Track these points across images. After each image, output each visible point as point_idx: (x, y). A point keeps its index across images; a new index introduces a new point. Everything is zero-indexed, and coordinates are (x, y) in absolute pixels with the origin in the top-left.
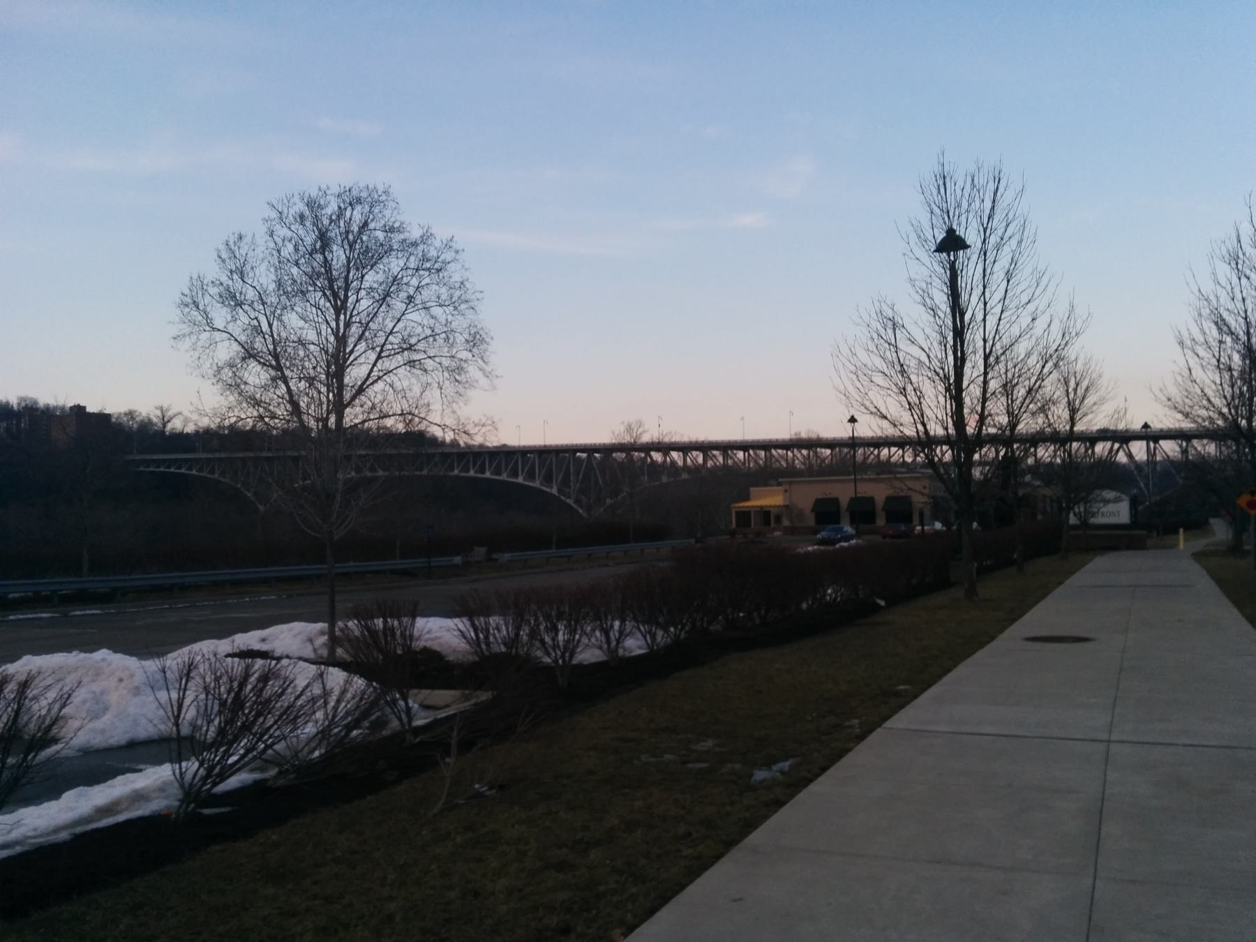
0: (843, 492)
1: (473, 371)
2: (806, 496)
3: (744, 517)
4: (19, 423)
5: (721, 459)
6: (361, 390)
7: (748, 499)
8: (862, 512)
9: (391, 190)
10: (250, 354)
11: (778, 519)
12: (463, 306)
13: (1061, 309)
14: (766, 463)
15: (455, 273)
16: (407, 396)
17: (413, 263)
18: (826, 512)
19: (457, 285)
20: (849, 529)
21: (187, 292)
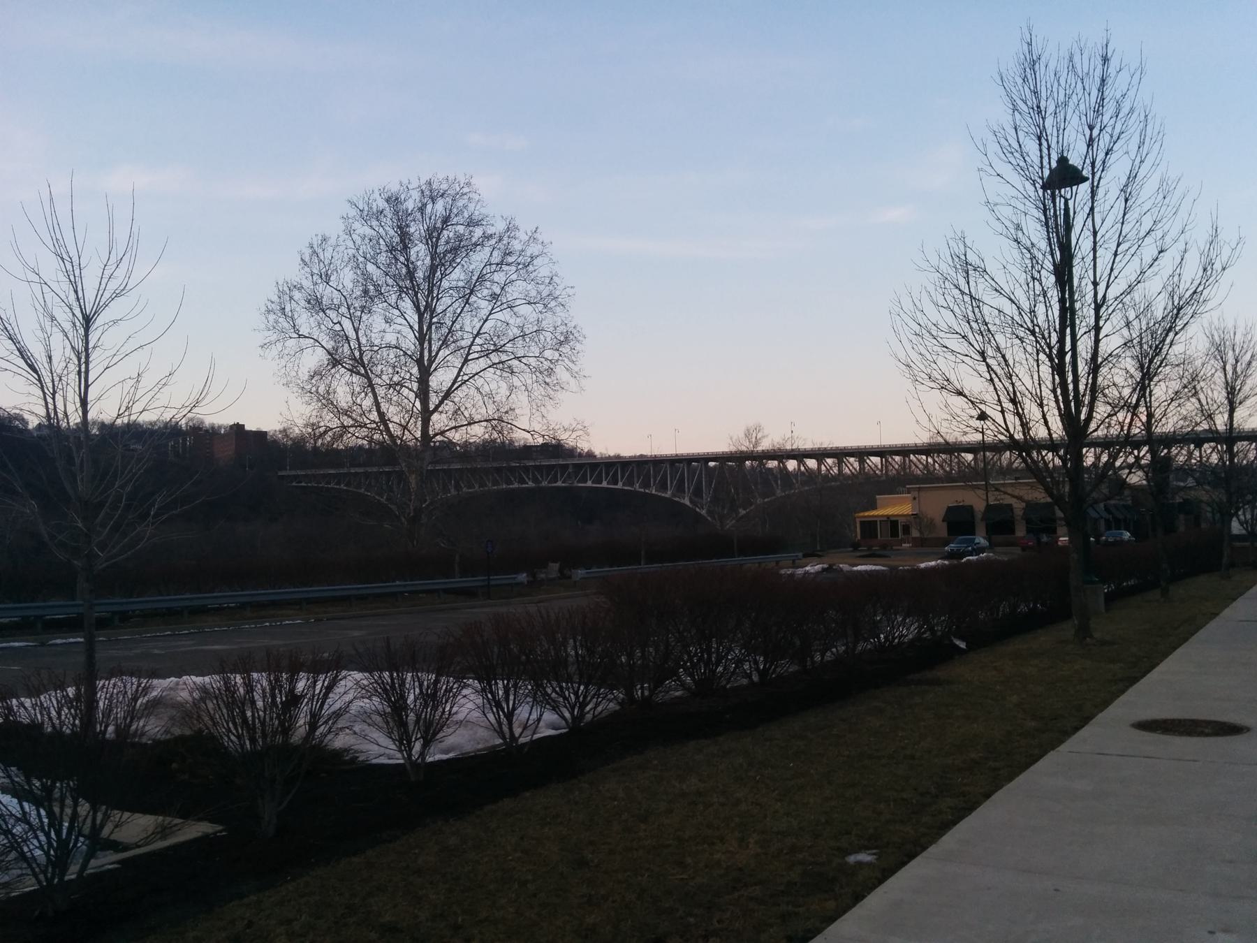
0: (976, 500)
1: (561, 373)
2: (937, 504)
3: (869, 527)
4: (184, 440)
5: (856, 465)
6: (447, 395)
7: (875, 508)
8: (999, 523)
9: (473, 181)
10: (335, 362)
11: (907, 529)
12: (553, 304)
13: (1199, 237)
14: (898, 468)
15: (542, 269)
16: (502, 404)
17: (496, 257)
18: (960, 522)
19: (547, 281)
20: (981, 540)
21: (275, 298)
